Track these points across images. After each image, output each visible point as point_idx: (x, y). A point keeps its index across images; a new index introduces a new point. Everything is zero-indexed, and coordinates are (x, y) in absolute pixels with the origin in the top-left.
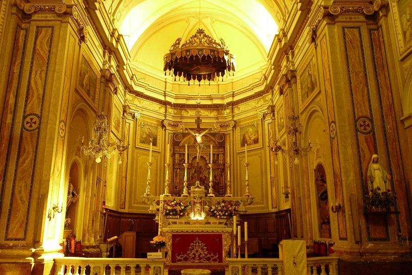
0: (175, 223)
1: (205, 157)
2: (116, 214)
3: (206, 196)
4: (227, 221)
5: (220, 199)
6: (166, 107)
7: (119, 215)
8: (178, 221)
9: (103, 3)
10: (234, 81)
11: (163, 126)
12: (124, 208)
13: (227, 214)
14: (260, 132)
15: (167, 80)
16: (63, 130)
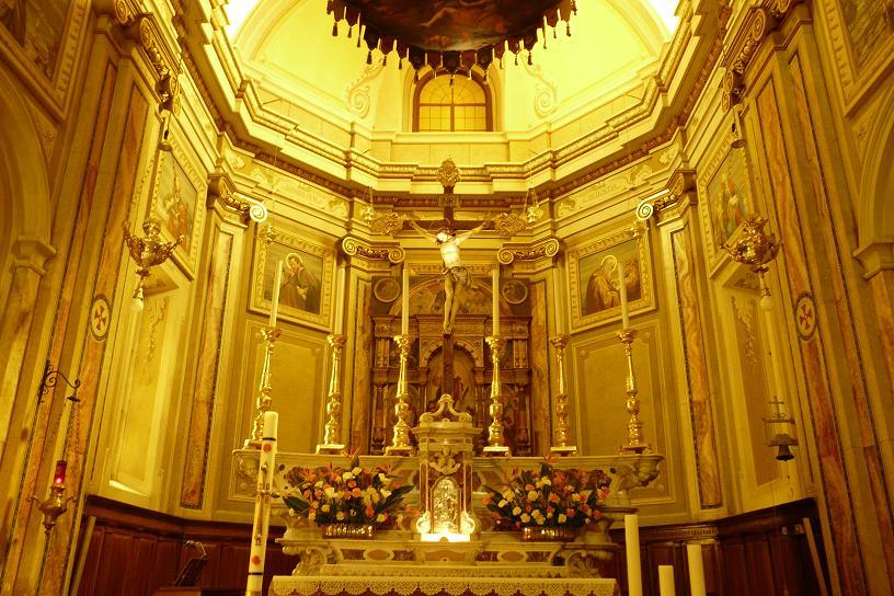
0: (357, 555)
1: (469, 348)
2: (161, 526)
3: (478, 452)
4: (563, 548)
5: (530, 463)
6: (351, 203)
7: (176, 529)
8: (367, 547)
9: (222, 29)
10: (553, 128)
11: (342, 257)
12: (199, 506)
13: (562, 518)
14: (645, 264)
15: (356, 129)
16: (104, 320)
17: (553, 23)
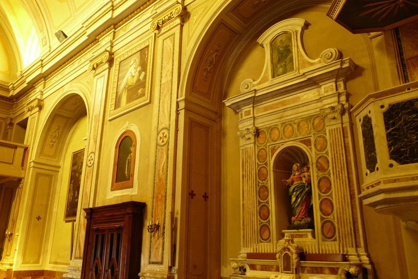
17: (226, 267)
